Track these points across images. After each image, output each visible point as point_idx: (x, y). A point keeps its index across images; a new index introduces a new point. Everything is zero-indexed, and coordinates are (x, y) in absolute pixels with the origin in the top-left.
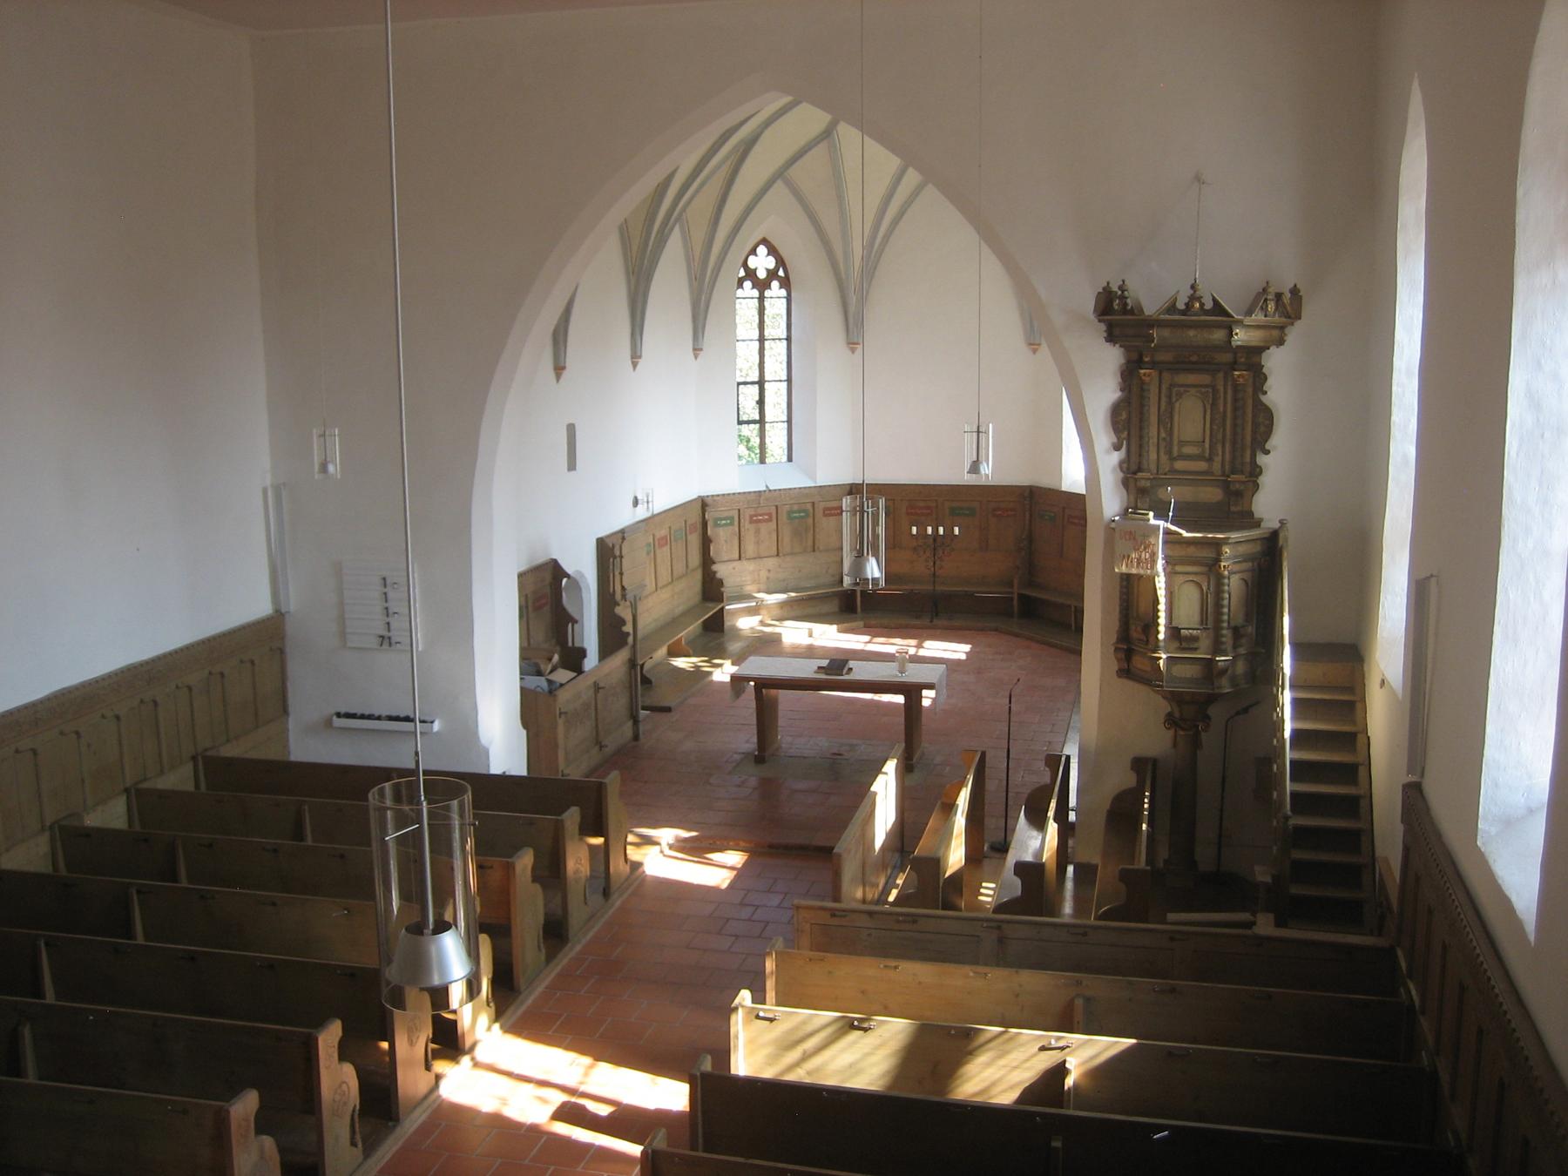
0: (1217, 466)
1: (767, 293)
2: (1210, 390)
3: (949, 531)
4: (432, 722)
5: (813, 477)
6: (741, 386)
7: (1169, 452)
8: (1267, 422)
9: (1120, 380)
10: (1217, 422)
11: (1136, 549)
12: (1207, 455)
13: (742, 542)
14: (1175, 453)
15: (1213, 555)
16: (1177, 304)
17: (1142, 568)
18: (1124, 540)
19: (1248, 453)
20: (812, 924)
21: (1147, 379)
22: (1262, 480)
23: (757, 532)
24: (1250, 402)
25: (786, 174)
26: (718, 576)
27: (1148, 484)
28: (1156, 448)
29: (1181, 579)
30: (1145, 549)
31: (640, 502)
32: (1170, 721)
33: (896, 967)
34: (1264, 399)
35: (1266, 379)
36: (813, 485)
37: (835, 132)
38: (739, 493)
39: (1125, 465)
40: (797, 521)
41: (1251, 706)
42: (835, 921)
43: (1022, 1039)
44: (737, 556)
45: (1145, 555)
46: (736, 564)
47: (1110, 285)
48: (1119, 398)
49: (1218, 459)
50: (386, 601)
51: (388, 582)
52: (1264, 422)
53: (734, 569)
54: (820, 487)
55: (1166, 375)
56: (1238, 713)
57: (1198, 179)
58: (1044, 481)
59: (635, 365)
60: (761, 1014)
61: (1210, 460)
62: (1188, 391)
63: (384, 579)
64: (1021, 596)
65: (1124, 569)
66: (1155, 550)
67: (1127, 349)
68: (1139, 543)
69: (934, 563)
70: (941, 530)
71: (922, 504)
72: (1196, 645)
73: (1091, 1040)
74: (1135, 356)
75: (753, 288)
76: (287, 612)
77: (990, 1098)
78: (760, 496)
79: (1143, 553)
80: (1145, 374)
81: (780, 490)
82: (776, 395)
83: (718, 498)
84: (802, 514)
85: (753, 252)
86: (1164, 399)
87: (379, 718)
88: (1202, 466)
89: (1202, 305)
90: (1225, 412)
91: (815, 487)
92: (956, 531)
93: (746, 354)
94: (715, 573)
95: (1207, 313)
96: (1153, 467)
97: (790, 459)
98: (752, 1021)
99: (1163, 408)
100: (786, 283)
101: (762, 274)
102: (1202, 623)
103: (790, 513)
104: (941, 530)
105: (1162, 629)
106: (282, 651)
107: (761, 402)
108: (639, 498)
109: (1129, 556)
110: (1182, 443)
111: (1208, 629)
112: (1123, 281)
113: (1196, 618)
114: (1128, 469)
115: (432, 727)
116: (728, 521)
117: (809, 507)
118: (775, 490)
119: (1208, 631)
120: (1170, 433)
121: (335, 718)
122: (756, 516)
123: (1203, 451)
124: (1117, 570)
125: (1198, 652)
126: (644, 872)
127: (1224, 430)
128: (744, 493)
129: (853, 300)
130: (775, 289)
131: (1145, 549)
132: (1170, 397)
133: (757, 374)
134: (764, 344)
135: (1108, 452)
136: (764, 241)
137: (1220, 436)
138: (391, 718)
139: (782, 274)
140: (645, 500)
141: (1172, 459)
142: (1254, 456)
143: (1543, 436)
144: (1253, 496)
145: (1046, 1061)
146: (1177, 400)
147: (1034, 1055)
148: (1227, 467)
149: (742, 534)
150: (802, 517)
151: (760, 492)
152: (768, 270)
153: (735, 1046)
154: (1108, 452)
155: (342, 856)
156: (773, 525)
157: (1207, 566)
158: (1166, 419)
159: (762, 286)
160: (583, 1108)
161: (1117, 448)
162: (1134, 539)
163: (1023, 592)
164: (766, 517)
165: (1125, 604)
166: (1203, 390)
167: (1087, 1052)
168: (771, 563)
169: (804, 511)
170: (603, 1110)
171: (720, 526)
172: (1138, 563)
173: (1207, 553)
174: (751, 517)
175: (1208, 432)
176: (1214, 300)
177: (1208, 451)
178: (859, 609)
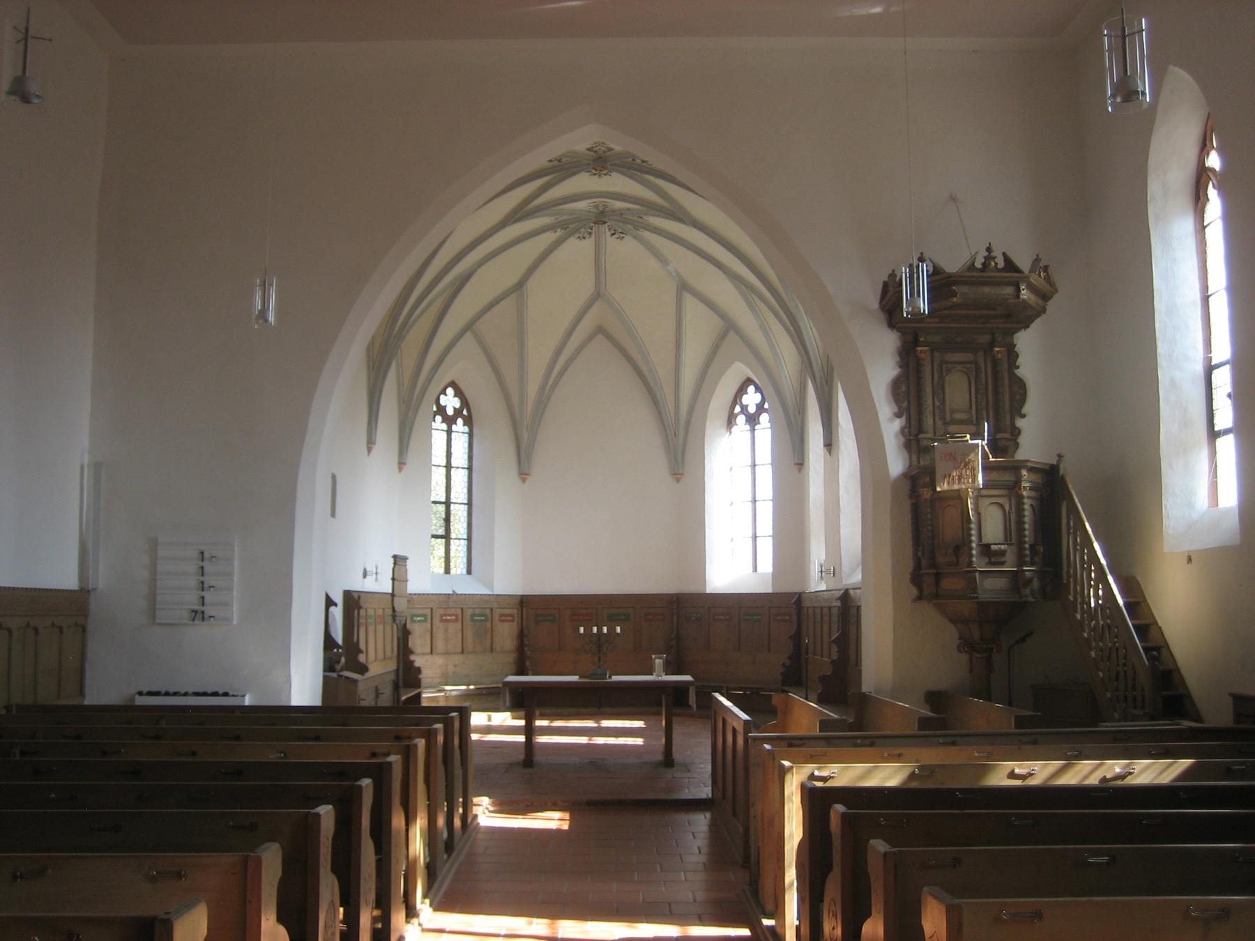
1: (454, 427)
2: (973, 366)
3: (612, 630)
4: (244, 696)
5: (489, 583)
6: (600, 336)
7: (943, 418)
8: (1021, 391)
9: (898, 359)
10: (981, 392)
11: (956, 468)
13: (434, 639)
14: (948, 418)
15: (1013, 478)
16: (975, 264)
17: (964, 483)
19: (1008, 417)
21: (923, 356)
23: (446, 630)
24: (1006, 376)
25: (474, 327)
26: (417, 664)
28: (932, 414)
29: (988, 501)
30: (965, 466)
31: (368, 573)
32: (967, 645)
34: (1017, 372)
35: (1017, 356)
36: (491, 593)
37: (525, 287)
38: (432, 594)
39: (906, 430)
40: (478, 623)
41: (1027, 636)
44: (428, 650)
46: (428, 657)
50: (203, 575)
51: (206, 555)
52: (1019, 390)
53: (427, 661)
54: (497, 595)
55: (937, 354)
57: (953, 199)
58: (689, 588)
59: (369, 450)
62: (955, 367)
63: (202, 553)
65: (946, 487)
68: (959, 460)
70: (605, 630)
71: (584, 611)
72: (1003, 560)
75: (442, 422)
76: (94, 590)
78: (449, 598)
79: (964, 471)
80: (921, 351)
81: (465, 595)
82: (459, 514)
83: (415, 597)
84: (483, 618)
85: (444, 392)
86: (936, 375)
87: (186, 694)
89: (996, 264)
90: (986, 383)
91: (493, 595)
92: (618, 629)
93: (438, 476)
94: (413, 662)
95: (999, 270)
96: (931, 430)
97: (469, 572)
100: (469, 421)
101: (450, 412)
103: (473, 615)
104: (605, 630)
106: (84, 629)
107: (447, 520)
108: (368, 569)
109: (950, 475)
110: (952, 412)
111: (1012, 544)
114: (910, 432)
115: (244, 701)
116: (423, 618)
117: (488, 612)
118: (461, 595)
119: (1012, 547)
120: (943, 401)
121: (137, 696)
122: (445, 615)
124: (938, 489)
126: (478, 824)
127: (987, 398)
128: (436, 594)
129: (525, 437)
130: (459, 426)
131: (965, 466)
133: (444, 495)
134: (450, 471)
135: (890, 420)
136: (453, 384)
137: (984, 404)
138: (197, 694)
139: (467, 413)
140: (374, 571)
141: (946, 424)
144: (1014, 453)
146: (947, 375)
149: (434, 631)
150: (481, 621)
151: (449, 594)
152: (455, 409)
153: (789, 817)
154: (890, 420)
156: (458, 625)
157: (1008, 489)
158: (939, 390)
159: (753, 420)
161: (898, 415)
162: (954, 459)
164: (454, 618)
166: (968, 366)
168: (458, 659)
169: (485, 615)
171: (415, 621)
172: (959, 480)
173: (1008, 477)
174: (442, 616)
177: (974, 417)
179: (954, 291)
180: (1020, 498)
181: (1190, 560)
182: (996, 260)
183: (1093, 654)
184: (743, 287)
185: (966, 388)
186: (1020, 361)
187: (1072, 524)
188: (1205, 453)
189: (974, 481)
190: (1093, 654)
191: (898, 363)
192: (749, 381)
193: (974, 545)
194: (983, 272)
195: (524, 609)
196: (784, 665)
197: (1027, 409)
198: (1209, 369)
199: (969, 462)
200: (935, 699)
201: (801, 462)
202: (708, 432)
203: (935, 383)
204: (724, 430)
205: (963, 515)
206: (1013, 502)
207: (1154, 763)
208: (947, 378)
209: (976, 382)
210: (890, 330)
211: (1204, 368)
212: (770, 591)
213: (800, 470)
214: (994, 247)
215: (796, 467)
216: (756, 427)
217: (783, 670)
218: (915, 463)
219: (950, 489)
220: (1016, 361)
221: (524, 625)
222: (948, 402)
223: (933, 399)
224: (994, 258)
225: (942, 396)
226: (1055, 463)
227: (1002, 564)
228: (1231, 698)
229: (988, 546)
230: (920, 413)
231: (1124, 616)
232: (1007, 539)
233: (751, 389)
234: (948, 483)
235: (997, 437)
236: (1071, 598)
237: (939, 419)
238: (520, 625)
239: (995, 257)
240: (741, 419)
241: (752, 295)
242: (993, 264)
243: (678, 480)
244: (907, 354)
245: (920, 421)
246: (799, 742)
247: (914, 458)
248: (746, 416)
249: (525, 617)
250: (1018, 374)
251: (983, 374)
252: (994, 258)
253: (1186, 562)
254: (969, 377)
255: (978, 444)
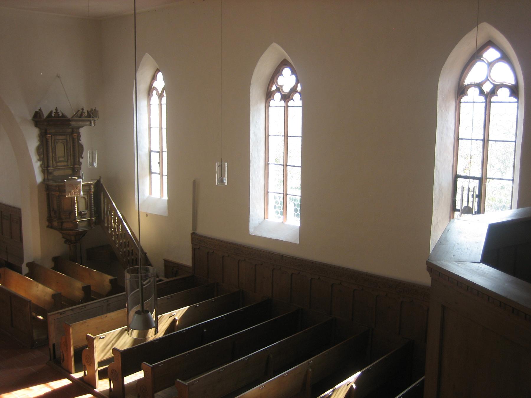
0: (69, 163)
7: (55, 160)
9: (39, 139)
11: (73, 189)
14: (57, 161)
17: (76, 194)
19: (77, 159)
24: (77, 143)
30: (77, 188)
34: (80, 142)
39: (43, 166)
42: (62, 316)
49: (69, 161)
52: (81, 147)
56: (274, 164)
60: (101, 337)
61: (67, 162)
65: (70, 196)
66: (80, 188)
67: (40, 129)
72: (85, 216)
73: (180, 310)
80: (48, 137)
88: (65, 164)
98: (98, 340)
102: (86, 209)
112: (95, 108)
114: (44, 166)
124: (67, 196)
127: (71, 153)
132: (55, 143)
135: (37, 162)
141: (57, 162)
145: (171, 319)
154: (37, 162)
162: (73, 186)
172: (75, 193)
181: (147, 215)
185: (63, 149)
187: (106, 201)
188: (148, 178)
193: (76, 213)
194: (81, 117)
197: (84, 155)
198: (150, 152)
199: (78, 187)
200: (56, 260)
203: (53, 147)
205: (72, 201)
206: (88, 196)
210: (36, 128)
211: (149, 151)
214: (84, 109)
218: (46, 178)
220: (80, 138)
222: (57, 154)
223: (52, 154)
225: (55, 152)
229: (81, 212)
230: (48, 159)
231: (132, 238)
232: (86, 208)
234: (70, 194)
235: (75, 167)
236: (106, 225)
242: (84, 114)
244: (43, 137)
245: (48, 162)
246: (64, 313)
252: (84, 113)
253: (146, 216)
254: (64, 145)
255: (81, 181)
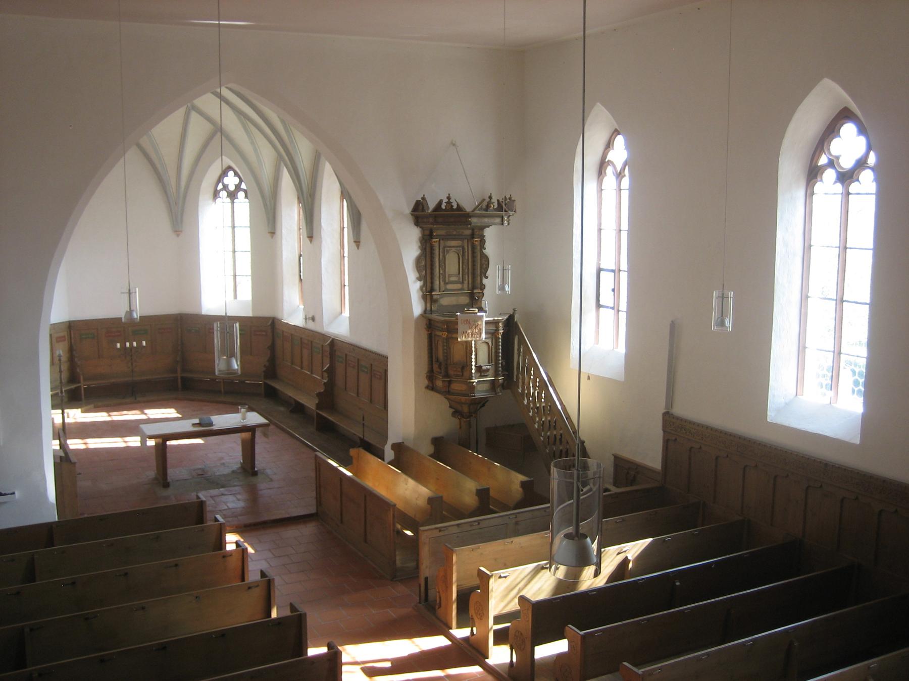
0: (466, 286)
3: (140, 344)
7: (444, 281)
9: (420, 245)
11: (470, 328)
12: (461, 280)
14: (447, 281)
18: (463, 324)
20: (430, 538)
22: (485, 291)
27: (438, 297)
30: (475, 328)
33: (512, 542)
39: (424, 289)
42: (442, 534)
43: (611, 552)
45: (475, 331)
47: (425, 196)
48: (420, 254)
49: (466, 282)
61: (462, 283)
64: (182, 378)
65: (464, 339)
66: (481, 327)
67: (423, 229)
68: (472, 325)
69: (132, 364)
70: (135, 344)
74: (427, 232)
77: (596, 585)
80: (434, 241)
88: (459, 286)
92: (144, 343)
96: (438, 289)
99: (441, 257)
104: (135, 344)
105: (473, 367)
110: (450, 276)
113: (487, 360)
114: (426, 289)
123: (459, 279)
124: (459, 340)
125: (489, 376)
131: (475, 328)
135: (415, 282)
137: (467, 271)
140: (307, 320)
141: (446, 284)
142: (481, 280)
143: (788, 256)
145: (620, 558)
146: (447, 254)
147: (615, 557)
148: (470, 286)
154: (415, 282)
155: (126, 574)
159: (232, 195)
160: (373, 668)
162: (469, 323)
163: (182, 375)
165: (446, 358)
166: (458, 248)
167: (635, 550)
170: (388, 665)
172: (472, 335)
175: (461, 269)
176: (458, 205)
178: (83, 397)
179: (470, 221)
180: (497, 339)
182: (494, 204)
183: (536, 426)
184: (242, 117)
186: (487, 245)
189: (480, 336)
190: (536, 426)
191: (419, 247)
192: (230, 168)
194: (487, 211)
195: (72, 331)
196: (265, 366)
201: (273, 231)
202: (200, 204)
204: (211, 201)
206: (494, 341)
207: (635, 545)
208: (447, 256)
209: (462, 258)
210: (416, 227)
212: (250, 315)
213: (272, 237)
215: (269, 234)
216: (235, 201)
217: (264, 369)
219: (466, 340)
221: (73, 341)
222: (447, 270)
224: (493, 203)
225: (444, 267)
226: (512, 314)
227: (486, 376)
228: (613, 457)
230: (432, 278)
233: (231, 173)
234: (465, 337)
237: (442, 281)
238: (69, 342)
239: (494, 203)
240: (223, 194)
241: (247, 122)
243: (178, 236)
244: (426, 242)
245: (432, 283)
246: (445, 529)
247: (428, 305)
248: (227, 192)
249: (72, 336)
250: (485, 253)
251: (467, 253)
252: (493, 203)
